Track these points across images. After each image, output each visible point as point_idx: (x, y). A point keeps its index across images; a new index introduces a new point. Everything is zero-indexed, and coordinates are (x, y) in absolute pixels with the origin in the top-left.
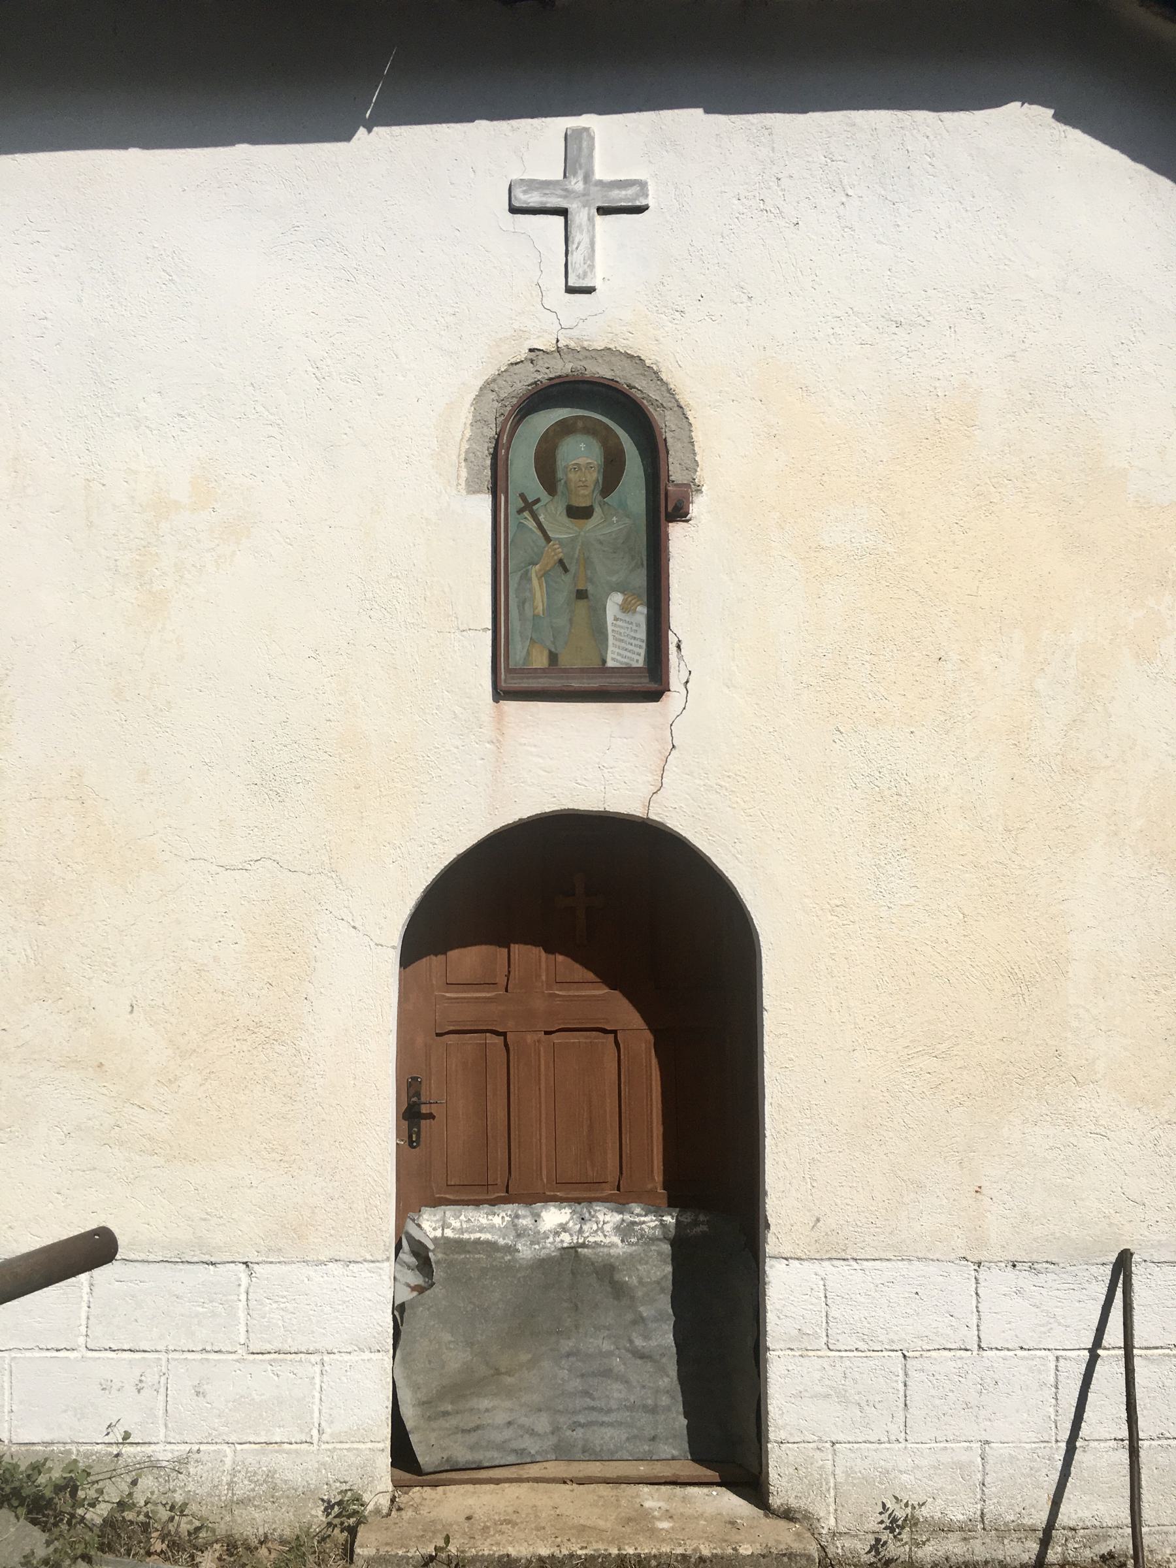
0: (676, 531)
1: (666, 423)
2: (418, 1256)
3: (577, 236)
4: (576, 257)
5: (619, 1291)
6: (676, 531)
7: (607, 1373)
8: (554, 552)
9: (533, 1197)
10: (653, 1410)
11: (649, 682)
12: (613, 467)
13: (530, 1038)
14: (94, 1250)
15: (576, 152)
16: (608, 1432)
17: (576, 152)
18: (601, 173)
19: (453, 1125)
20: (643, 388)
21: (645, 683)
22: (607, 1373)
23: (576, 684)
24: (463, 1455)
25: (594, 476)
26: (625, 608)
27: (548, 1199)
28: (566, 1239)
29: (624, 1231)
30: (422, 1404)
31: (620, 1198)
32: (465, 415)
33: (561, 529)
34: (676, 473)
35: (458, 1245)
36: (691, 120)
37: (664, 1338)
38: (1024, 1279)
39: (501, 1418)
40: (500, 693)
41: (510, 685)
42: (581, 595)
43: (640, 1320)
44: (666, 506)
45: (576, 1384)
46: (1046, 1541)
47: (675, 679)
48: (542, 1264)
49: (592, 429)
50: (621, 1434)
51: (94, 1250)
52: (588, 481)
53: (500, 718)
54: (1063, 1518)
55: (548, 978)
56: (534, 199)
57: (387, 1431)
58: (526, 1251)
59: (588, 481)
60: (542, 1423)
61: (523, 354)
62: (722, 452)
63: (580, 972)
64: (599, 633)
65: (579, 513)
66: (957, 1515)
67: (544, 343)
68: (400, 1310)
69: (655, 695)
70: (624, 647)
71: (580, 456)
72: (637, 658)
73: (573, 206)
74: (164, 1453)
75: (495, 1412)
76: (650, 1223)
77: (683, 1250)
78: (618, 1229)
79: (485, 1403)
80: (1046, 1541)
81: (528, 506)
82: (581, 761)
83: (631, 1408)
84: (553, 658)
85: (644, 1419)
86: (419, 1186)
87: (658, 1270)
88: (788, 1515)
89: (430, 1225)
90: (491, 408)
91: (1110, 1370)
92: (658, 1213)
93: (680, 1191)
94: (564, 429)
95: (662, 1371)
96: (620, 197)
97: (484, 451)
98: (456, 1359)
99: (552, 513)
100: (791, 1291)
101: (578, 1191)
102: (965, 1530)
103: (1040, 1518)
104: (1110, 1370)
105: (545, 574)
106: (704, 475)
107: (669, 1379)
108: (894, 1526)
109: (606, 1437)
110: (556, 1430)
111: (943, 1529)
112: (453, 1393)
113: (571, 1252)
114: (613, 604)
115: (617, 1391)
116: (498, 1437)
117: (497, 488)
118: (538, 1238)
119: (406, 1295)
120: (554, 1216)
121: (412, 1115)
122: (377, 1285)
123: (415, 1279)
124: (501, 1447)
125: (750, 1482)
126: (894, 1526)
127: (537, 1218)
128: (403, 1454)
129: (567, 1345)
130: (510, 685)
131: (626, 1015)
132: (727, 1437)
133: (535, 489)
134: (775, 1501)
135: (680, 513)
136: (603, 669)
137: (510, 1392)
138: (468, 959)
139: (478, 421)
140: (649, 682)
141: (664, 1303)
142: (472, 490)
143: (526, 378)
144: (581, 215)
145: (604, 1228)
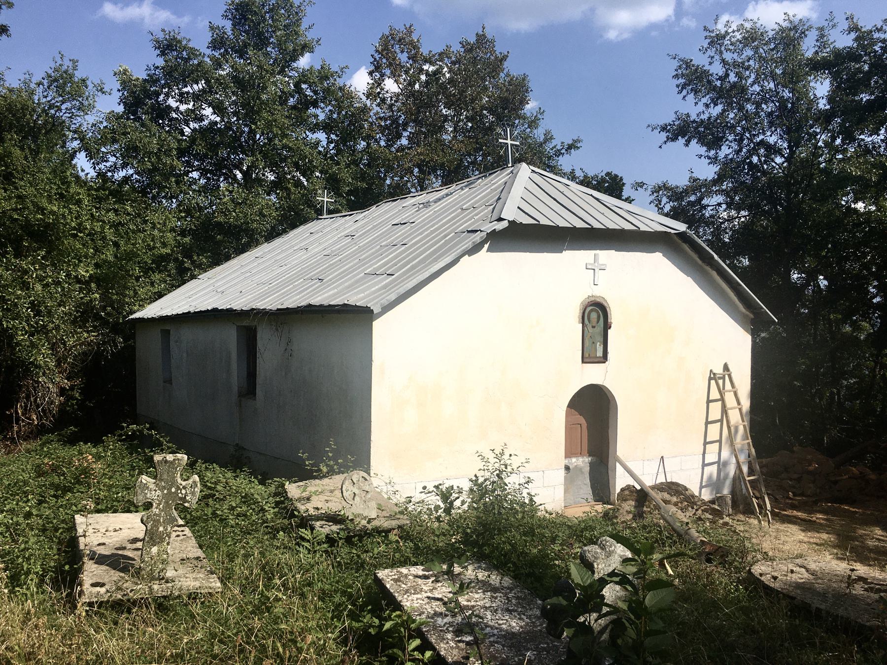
44: (607, 326)
49: (598, 312)
52: (596, 316)
59: (596, 316)
62: (615, 317)
65: (593, 327)
70: (600, 353)
71: (594, 316)
82: (594, 375)
96: (603, 267)
135: (610, 328)
140: (604, 358)
144: (597, 270)
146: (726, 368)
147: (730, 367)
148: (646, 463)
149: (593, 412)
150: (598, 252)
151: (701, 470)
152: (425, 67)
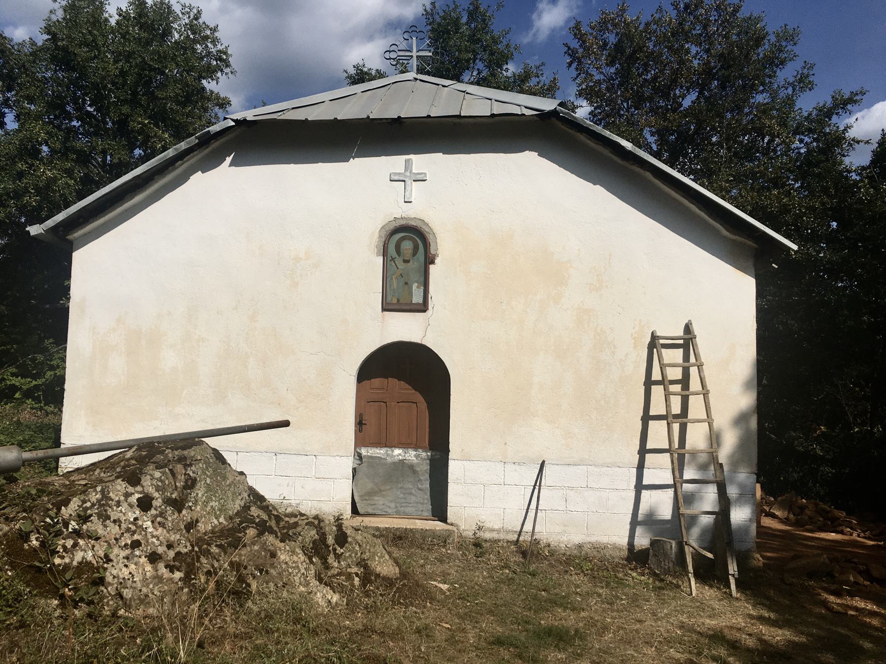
0: (431, 266)
1: (430, 238)
2: (360, 457)
3: (407, 188)
4: (407, 193)
5: (415, 472)
6: (431, 266)
7: (411, 494)
8: (399, 272)
10: (423, 504)
11: (423, 308)
13: (393, 404)
14: (286, 424)
15: (408, 163)
16: (410, 509)
17: (408, 163)
19: (371, 428)
20: (425, 228)
21: (422, 308)
22: (411, 494)
23: (403, 308)
24: (371, 511)
25: (411, 251)
26: (418, 287)
27: (395, 447)
28: (401, 458)
29: (417, 456)
30: (361, 496)
31: (416, 448)
32: (377, 235)
34: (432, 252)
35: (371, 457)
36: (439, 156)
37: (427, 485)
38: (517, 467)
39: (381, 502)
40: (384, 309)
41: (387, 307)
42: (406, 283)
43: (420, 480)
44: (430, 260)
45: (401, 496)
46: (519, 535)
47: (430, 307)
48: (394, 463)
49: (410, 239)
50: (413, 509)
51: (286, 424)
52: (408, 251)
53: (383, 316)
54: (524, 529)
55: (398, 387)
56: (396, 178)
57: (350, 499)
58: (389, 460)
59: (408, 251)
60: (393, 505)
61: (392, 219)
62: (445, 247)
63: (407, 386)
64: (411, 294)
65: (406, 261)
66: (496, 527)
67: (398, 216)
68: (354, 470)
69: (425, 311)
70: (417, 298)
71: (407, 246)
72: (421, 301)
73: (407, 180)
75: (379, 501)
76: (424, 454)
77: (433, 462)
78: (415, 456)
79: (376, 498)
80: (519, 535)
81: (393, 259)
82: (404, 328)
83: (417, 503)
84: (398, 300)
85: (420, 506)
86: (361, 439)
87: (426, 467)
88: (452, 525)
89: (364, 451)
90: (384, 233)
91: (536, 491)
92: (426, 452)
93: (432, 447)
94: (403, 239)
95: (426, 494)
96: (419, 177)
97: (382, 244)
98: (370, 486)
99: (399, 261)
100: (454, 468)
101: (405, 445)
102: (498, 531)
103: (519, 529)
104: (536, 491)
105: (396, 278)
106: (440, 252)
107: (427, 496)
108: (480, 529)
109: (409, 510)
110: (396, 507)
111: (493, 530)
112: (369, 494)
113: (402, 462)
114: (415, 285)
115: (413, 499)
116: (380, 507)
117: (385, 253)
118: (393, 456)
119: (356, 466)
121: (360, 423)
122: (348, 463)
123: (359, 462)
124: (381, 510)
125: (443, 518)
126: (480, 529)
127: (393, 451)
128: (355, 511)
129: (400, 486)
130: (387, 307)
131: (419, 398)
132: (440, 511)
133: (395, 255)
134: (449, 521)
135: (432, 262)
136: (411, 304)
137: (384, 496)
138: (377, 382)
139: (380, 236)
140: (423, 308)
141: (427, 476)
142: (378, 255)
143: (392, 227)
144: (408, 182)
145: (411, 455)
146: (688, 329)
147: (701, 342)
148: (509, 467)
149: (407, 389)
150: (411, 156)
151: (632, 494)
152: (68, 483)
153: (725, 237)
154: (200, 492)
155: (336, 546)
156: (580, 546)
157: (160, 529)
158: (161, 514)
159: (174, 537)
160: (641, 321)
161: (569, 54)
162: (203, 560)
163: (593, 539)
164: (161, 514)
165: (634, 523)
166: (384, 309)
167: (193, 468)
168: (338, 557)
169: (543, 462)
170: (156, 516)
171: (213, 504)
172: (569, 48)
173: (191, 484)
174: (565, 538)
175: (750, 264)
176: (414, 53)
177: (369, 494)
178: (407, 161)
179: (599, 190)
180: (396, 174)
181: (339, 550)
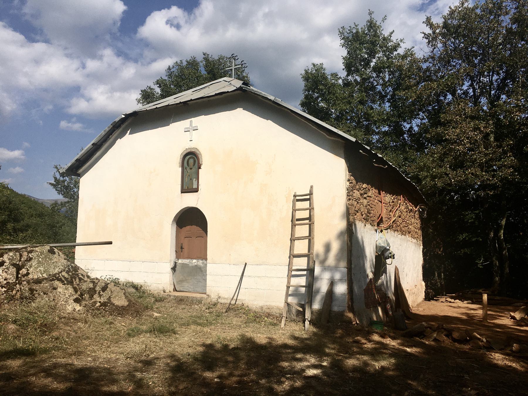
1: (200, 156)
8: (188, 174)
9: (192, 259)
11: (196, 191)
12: (195, 161)
14: (110, 243)
18: (193, 126)
24: (182, 290)
25: (193, 164)
33: (189, 170)
40: (182, 192)
41: (183, 191)
44: (200, 168)
48: (193, 267)
51: (110, 243)
54: (201, 291)
56: (186, 130)
60: (192, 287)
65: (191, 169)
66: (226, 297)
69: (197, 191)
71: (191, 161)
74: (149, 284)
82: (190, 201)
99: (188, 169)
112: (181, 282)
120: (194, 261)
128: (175, 290)
130: (183, 191)
137: (187, 282)
150: (193, 119)
151: (286, 280)
153: (329, 139)
154: (34, 263)
155: (101, 292)
156: (262, 308)
157: (4, 273)
158: (7, 268)
159: (8, 277)
160: (289, 188)
161: (426, 38)
162: (18, 286)
163: (268, 304)
164: (7, 268)
165: (287, 295)
166: (182, 192)
167: (32, 254)
168: (100, 296)
169: (246, 264)
170: (5, 269)
171: (41, 269)
172: (425, 34)
173: (30, 259)
174: (255, 303)
175: (342, 152)
176: (233, 68)
177: (181, 282)
178: (191, 121)
179: (270, 122)
180: (186, 128)
181: (102, 293)
